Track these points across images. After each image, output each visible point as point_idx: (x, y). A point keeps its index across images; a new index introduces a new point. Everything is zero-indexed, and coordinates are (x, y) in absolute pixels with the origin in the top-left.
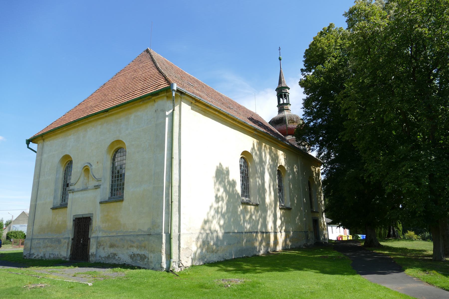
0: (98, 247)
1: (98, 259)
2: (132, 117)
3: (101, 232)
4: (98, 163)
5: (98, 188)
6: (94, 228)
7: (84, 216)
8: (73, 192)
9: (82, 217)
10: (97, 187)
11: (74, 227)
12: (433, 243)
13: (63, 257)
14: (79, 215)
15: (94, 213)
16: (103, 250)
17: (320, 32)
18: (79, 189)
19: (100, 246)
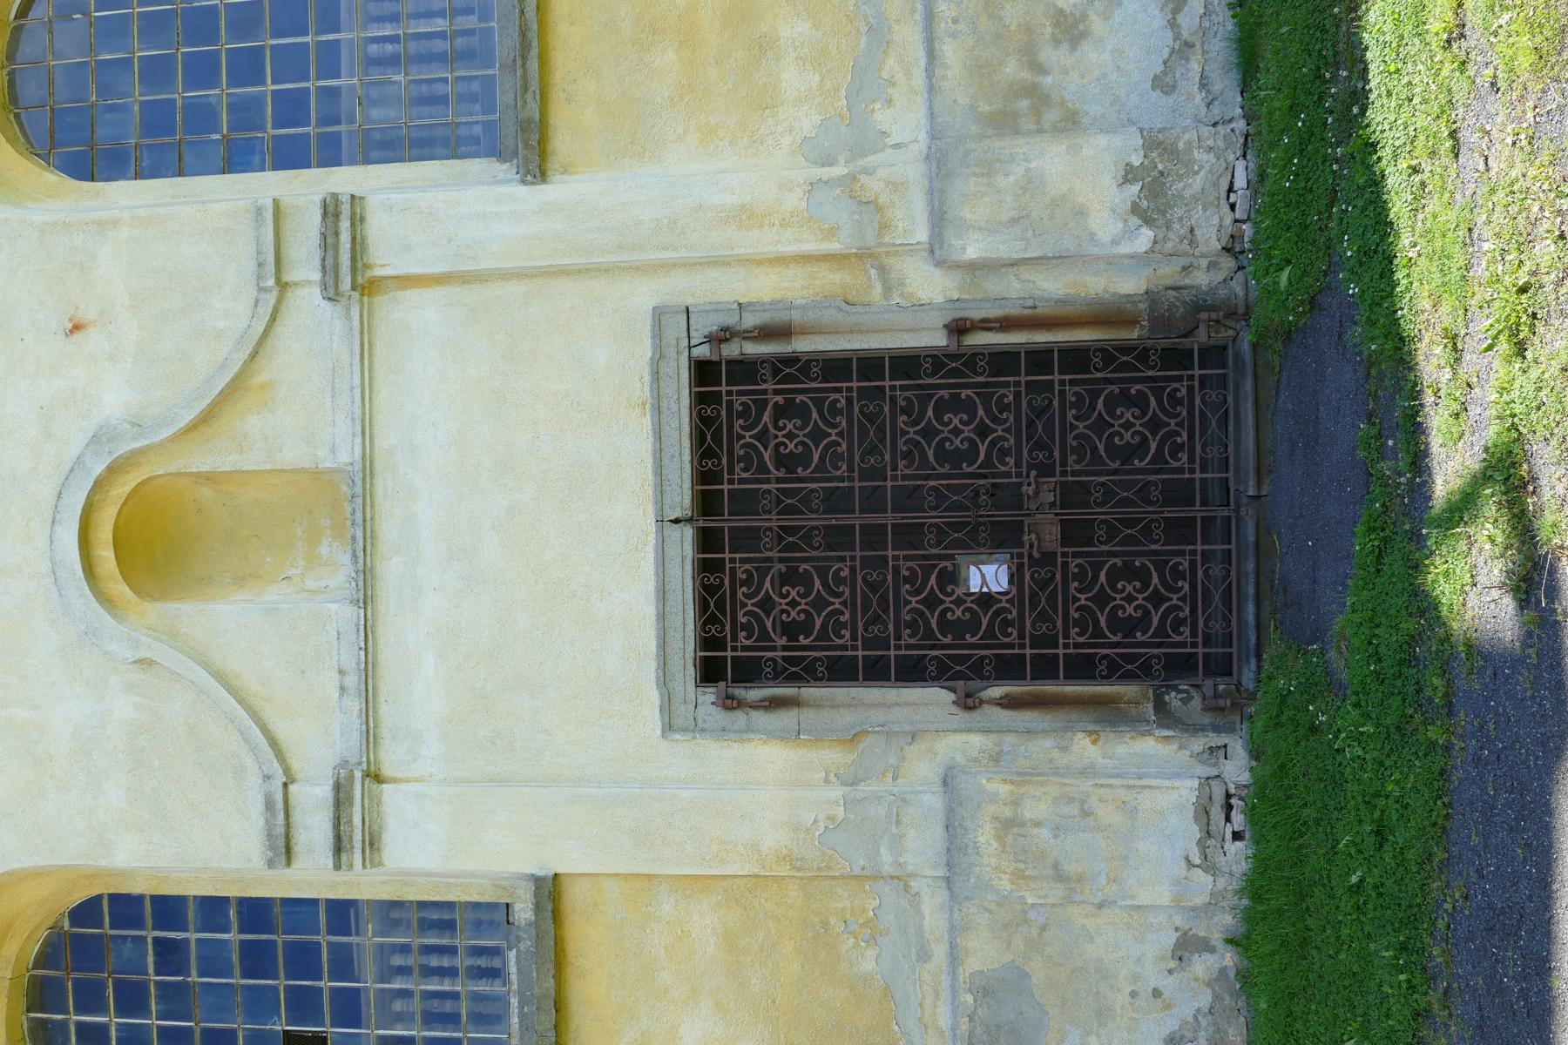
0: (1052, 116)
1: (1199, 98)
2: (573, 961)
3: (883, 117)
4: (77, 328)
5: (357, 220)
6: (831, 233)
7: (682, 498)
8: (378, 779)
9: (688, 532)
10: (345, 225)
11: (809, 692)
12: (1080, 735)
13: (1208, 866)
14: (662, 594)
15: (644, 295)
16: (1086, 46)
17: (709, 695)
18: (352, 681)
19: (1040, 99)
